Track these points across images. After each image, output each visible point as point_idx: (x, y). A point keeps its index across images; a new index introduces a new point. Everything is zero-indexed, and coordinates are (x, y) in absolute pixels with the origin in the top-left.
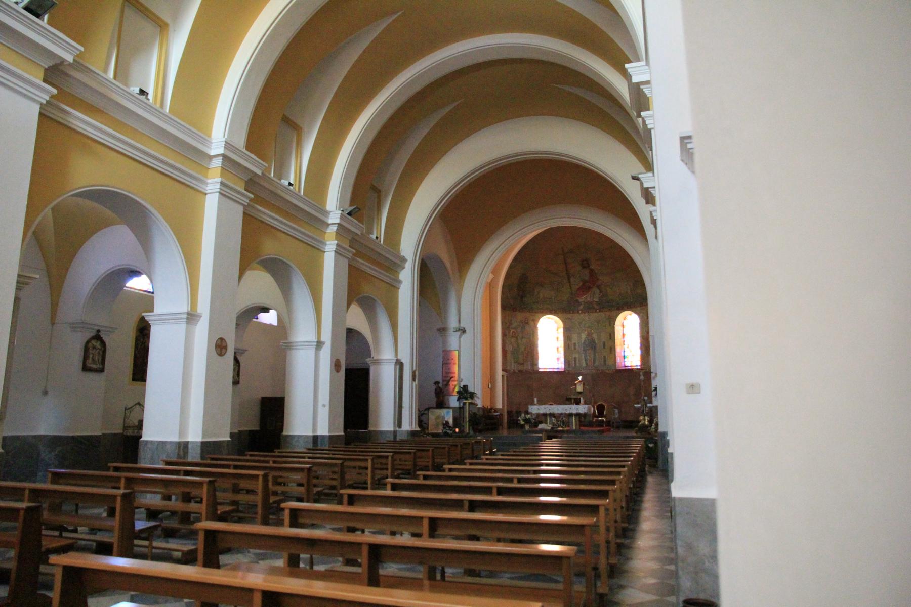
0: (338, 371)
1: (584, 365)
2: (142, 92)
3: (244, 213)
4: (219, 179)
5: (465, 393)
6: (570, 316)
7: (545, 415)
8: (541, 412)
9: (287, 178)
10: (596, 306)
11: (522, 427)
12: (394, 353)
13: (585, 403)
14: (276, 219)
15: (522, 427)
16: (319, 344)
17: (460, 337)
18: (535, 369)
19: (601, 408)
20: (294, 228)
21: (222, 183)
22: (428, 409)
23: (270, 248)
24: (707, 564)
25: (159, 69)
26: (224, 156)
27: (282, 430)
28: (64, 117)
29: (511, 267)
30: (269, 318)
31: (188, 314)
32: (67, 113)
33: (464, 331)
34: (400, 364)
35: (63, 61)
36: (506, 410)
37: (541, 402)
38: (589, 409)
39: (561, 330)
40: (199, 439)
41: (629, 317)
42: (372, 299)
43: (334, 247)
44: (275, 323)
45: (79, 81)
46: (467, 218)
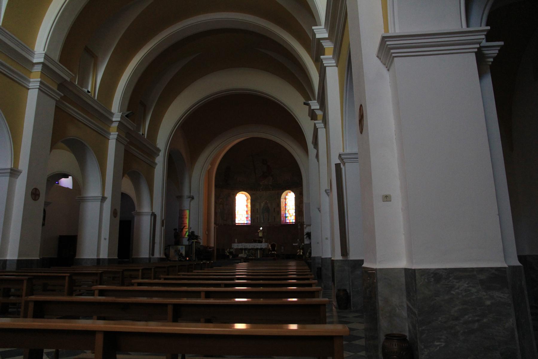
0: (115, 217)
1: (262, 221)
3: (56, 106)
4: (39, 79)
5: (192, 236)
7: (242, 249)
8: (239, 247)
9: (87, 88)
11: (228, 256)
12: (150, 207)
13: (266, 242)
14: (79, 114)
15: (228, 256)
16: (103, 199)
17: (190, 202)
19: (273, 246)
20: (90, 121)
22: (169, 246)
23: (73, 132)
24: (398, 311)
27: (75, 254)
30: (67, 182)
31: (11, 169)
33: (193, 198)
34: (154, 215)
36: (215, 248)
37: (239, 242)
38: (268, 246)
40: (16, 258)
44: (71, 187)
46: (196, 130)
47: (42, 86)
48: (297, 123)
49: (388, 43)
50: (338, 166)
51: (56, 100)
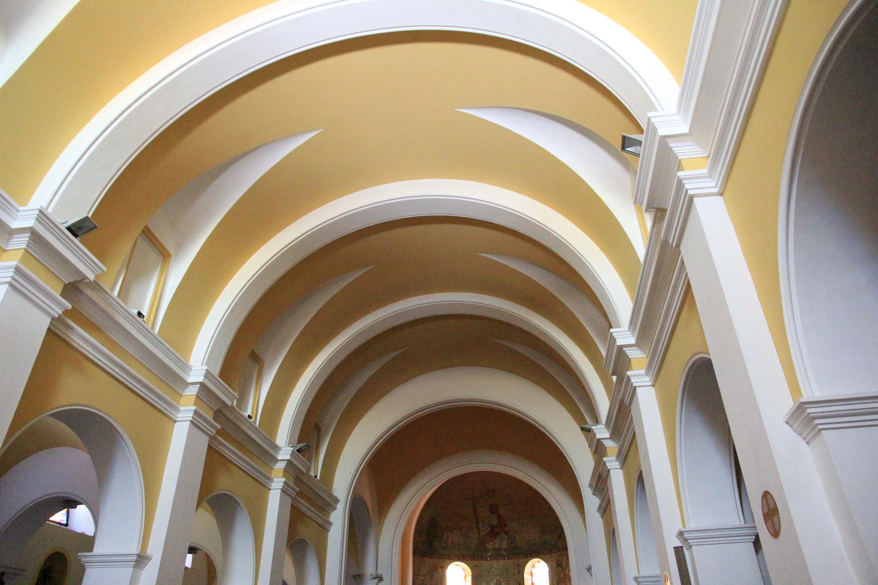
2: (140, 314)
3: (209, 446)
4: (194, 408)
6: (478, 563)
10: (504, 553)
20: (247, 463)
21: (196, 412)
23: (225, 483)
25: (156, 294)
26: (202, 385)
28: (67, 332)
29: (422, 511)
31: (139, 556)
32: (72, 328)
35: (85, 277)
39: (469, 578)
41: (537, 565)
42: (306, 542)
43: (281, 485)
45: (90, 299)
47: (196, 417)
48: (564, 457)
49: (809, 411)
50: (678, 551)
51: (210, 436)
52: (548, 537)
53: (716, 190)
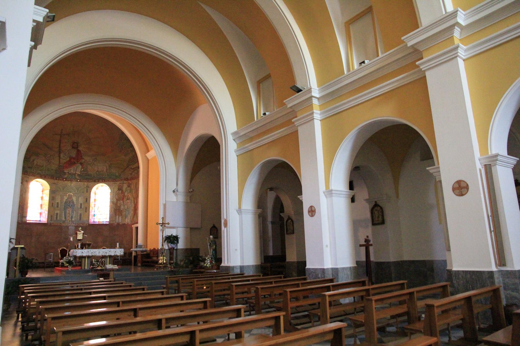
6: (56, 181)
13: (120, 247)
18: (24, 220)
41: (100, 188)
52: (113, 171)
53: (464, 58)
